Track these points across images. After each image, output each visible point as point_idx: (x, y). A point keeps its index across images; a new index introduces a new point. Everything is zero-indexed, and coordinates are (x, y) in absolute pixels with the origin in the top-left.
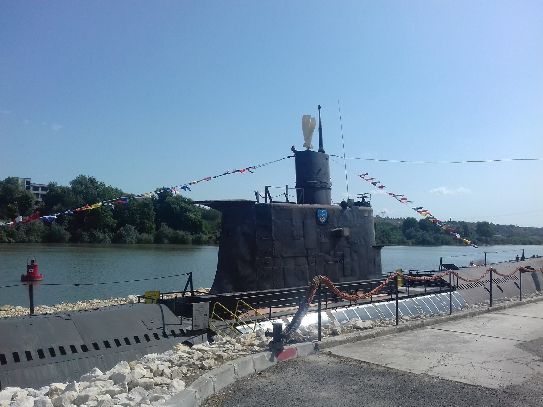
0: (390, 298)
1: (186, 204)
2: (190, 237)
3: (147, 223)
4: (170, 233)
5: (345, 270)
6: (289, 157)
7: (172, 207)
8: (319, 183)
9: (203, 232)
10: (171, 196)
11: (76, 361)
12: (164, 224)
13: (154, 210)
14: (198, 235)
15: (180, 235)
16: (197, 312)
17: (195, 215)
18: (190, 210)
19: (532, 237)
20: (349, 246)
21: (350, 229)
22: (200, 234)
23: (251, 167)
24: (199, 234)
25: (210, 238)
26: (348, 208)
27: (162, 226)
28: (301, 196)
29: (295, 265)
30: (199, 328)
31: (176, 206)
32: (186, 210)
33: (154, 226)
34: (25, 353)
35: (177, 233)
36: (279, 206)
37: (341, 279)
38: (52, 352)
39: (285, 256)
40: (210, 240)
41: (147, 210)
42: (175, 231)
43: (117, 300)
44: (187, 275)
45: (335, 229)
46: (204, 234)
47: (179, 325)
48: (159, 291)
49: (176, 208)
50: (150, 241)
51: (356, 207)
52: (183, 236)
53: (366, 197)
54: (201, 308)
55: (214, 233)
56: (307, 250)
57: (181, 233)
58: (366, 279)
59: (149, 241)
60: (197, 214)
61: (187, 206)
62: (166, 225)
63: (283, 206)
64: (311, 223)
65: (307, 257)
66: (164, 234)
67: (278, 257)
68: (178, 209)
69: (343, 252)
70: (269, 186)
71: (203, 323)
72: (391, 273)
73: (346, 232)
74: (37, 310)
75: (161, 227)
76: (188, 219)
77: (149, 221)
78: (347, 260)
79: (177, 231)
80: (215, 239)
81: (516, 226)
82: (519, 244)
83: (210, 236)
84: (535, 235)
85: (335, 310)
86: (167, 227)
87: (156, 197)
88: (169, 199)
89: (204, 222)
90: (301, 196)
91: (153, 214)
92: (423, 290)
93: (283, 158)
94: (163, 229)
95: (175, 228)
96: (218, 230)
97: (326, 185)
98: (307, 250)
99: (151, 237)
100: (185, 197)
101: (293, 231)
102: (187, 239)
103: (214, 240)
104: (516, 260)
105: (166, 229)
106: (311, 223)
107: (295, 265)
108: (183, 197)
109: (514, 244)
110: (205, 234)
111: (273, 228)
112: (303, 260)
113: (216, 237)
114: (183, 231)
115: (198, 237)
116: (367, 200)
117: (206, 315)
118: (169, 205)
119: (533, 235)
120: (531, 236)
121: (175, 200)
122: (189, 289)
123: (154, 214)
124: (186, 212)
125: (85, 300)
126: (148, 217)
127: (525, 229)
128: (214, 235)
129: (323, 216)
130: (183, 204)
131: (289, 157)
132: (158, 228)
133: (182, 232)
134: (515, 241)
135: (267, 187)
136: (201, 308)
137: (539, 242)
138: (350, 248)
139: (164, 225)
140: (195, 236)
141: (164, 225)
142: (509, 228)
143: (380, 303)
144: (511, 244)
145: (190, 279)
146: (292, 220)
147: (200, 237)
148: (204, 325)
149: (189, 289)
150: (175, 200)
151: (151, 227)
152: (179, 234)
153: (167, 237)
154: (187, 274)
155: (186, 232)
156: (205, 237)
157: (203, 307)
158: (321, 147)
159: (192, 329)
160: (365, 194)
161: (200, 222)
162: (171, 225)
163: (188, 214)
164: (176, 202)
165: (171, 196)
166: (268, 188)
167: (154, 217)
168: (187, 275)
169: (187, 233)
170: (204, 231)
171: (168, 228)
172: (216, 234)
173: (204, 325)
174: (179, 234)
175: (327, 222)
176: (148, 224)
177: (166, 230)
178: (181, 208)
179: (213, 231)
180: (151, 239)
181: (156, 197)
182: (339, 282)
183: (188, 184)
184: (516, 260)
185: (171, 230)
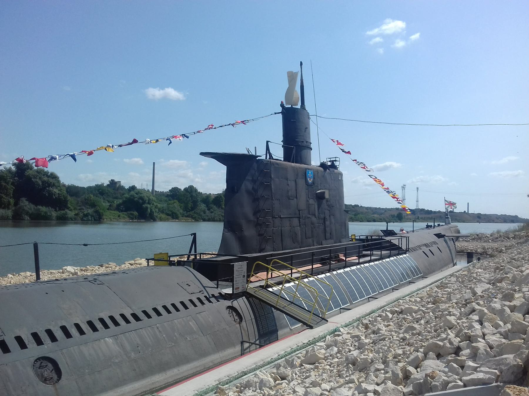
0: (358, 262)
1: (49, 178)
2: (54, 214)
3: (4, 198)
4: (31, 209)
5: (326, 233)
6: (276, 113)
7: (33, 181)
8: (305, 142)
9: (68, 208)
10: (31, 170)
11: (134, 333)
12: (24, 199)
13: (13, 184)
14: (62, 212)
15: (42, 211)
16: (237, 273)
17: (59, 190)
18: (54, 185)
19: (373, 215)
20: (328, 208)
21: (329, 191)
22: (66, 210)
23: (245, 121)
24: (64, 210)
25: (76, 215)
26: (327, 170)
27: (21, 201)
28: (293, 154)
29: (290, 226)
30: (238, 291)
31: (37, 180)
32: (50, 185)
33: (12, 201)
34: (74, 326)
35: (39, 209)
36: (277, 164)
37: (324, 242)
38: (137, 318)
39: (282, 217)
40: (76, 217)
41: (4, 184)
42: (36, 207)
43: (53, 273)
44: (192, 236)
45: (319, 191)
46: (69, 211)
47: (215, 288)
48: (168, 253)
49: (37, 182)
50: (8, 217)
51: (333, 170)
52: (46, 213)
53: (336, 161)
54: (241, 268)
55: (80, 209)
56: (299, 211)
57: (43, 209)
58: (340, 242)
59: (6, 217)
60: (61, 189)
61: (50, 180)
62: (26, 200)
63: (281, 164)
64: (301, 182)
65: (299, 218)
66: (24, 210)
67: (277, 218)
68: (41, 183)
69: (325, 214)
70: (269, 141)
71: (242, 286)
72: (360, 236)
73: (327, 196)
74: (45, 276)
75: (20, 203)
76: (51, 194)
77: (7, 195)
78: (327, 223)
79: (40, 207)
80: (81, 216)
81: (360, 206)
82: (365, 221)
83: (77, 212)
84: (375, 213)
85: (336, 272)
86: (27, 203)
87: (13, 168)
88: (29, 173)
89: (69, 198)
90: (293, 154)
91: (11, 188)
92: (310, 267)
93: (272, 114)
94: (22, 204)
95: (36, 203)
96: (84, 206)
97: (309, 145)
98: (299, 211)
99: (9, 213)
100: (48, 171)
101: (288, 191)
102: (50, 215)
103: (81, 217)
104: (426, 228)
105: (25, 204)
106: (301, 182)
107: (290, 226)
108: (45, 170)
109: (361, 222)
110: (71, 210)
111: (273, 187)
112: (296, 221)
113: (83, 214)
114: (46, 206)
115: (63, 214)
116: (336, 164)
117: (244, 277)
118: (29, 179)
119: (373, 214)
120: (372, 214)
121: (36, 173)
122: (193, 252)
123: (12, 188)
124: (49, 186)
125: (14, 273)
126: (5, 191)
127: (367, 208)
128: (80, 212)
129: (310, 176)
130: (45, 179)
131: (276, 113)
132: (16, 204)
133: (45, 207)
134: (361, 218)
135: (267, 142)
136: (241, 268)
137: (381, 219)
138: (329, 211)
139: (24, 200)
140: (59, 212)
141: (24, 200)
142: (354, 208)
143: (364, 265)
144: (358, 221)
145: (194, 241)
146: (287, 179)
147: (66, 214)
148: (243, 287)
149: (193, 252)
150: (36, 173)
151: (9, 202)
152: (41, 210)
153: (27, 213)
154: (191, 234)
155: (49, 208)
156: (71, 214)
157: (242, 268)
158: (304, 106)
159: (233, 292)
160: (336, 158)
161: (65, 198)
162: (31, 201)
163: (52, 189)
164: (38, 176)
165: (31, 170)
166: (269, 143)
167: (12, 191)
168: (192, 236)
169: (51, 210)
170: (70, 208)
171: (29, 203)
172: (83, 211)
173: (243, 287)
174: (41, 210)
175: (313, 183)
176: (5, 199)
177: (26, 206)
178: (43, 182)
179: (79, 208)
180: (9, 215)
181: (13, 168)
182: (322, 245)
183: (192, 134)
184: (426, 228)
185: (32, 206)
